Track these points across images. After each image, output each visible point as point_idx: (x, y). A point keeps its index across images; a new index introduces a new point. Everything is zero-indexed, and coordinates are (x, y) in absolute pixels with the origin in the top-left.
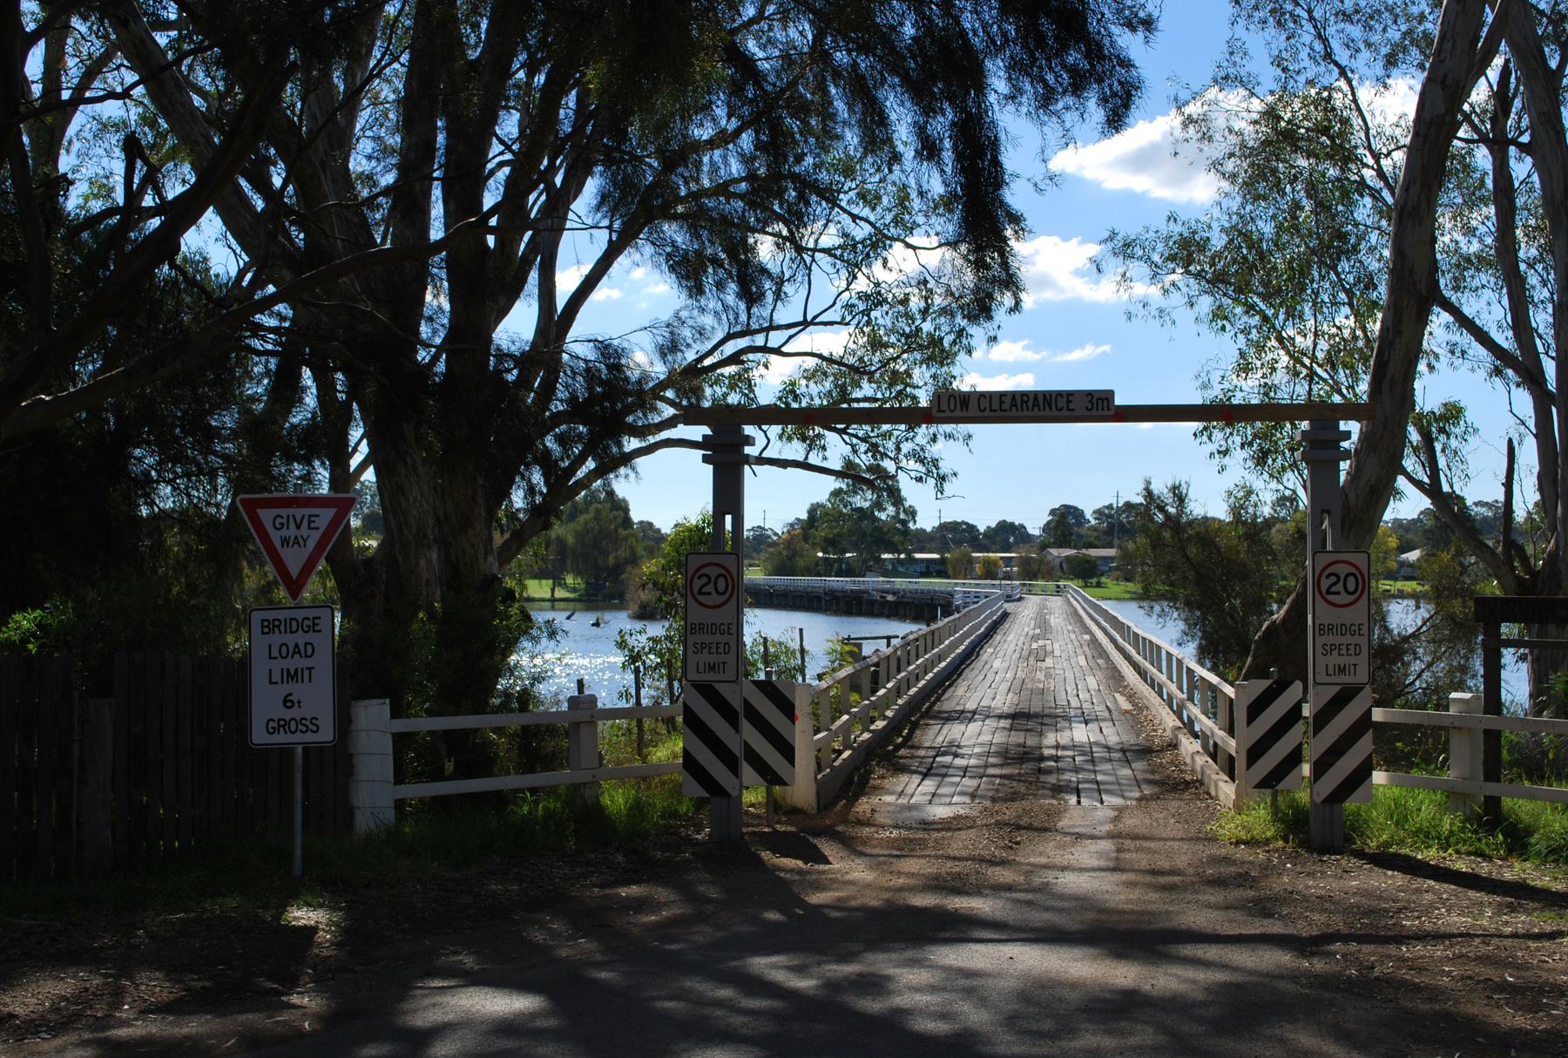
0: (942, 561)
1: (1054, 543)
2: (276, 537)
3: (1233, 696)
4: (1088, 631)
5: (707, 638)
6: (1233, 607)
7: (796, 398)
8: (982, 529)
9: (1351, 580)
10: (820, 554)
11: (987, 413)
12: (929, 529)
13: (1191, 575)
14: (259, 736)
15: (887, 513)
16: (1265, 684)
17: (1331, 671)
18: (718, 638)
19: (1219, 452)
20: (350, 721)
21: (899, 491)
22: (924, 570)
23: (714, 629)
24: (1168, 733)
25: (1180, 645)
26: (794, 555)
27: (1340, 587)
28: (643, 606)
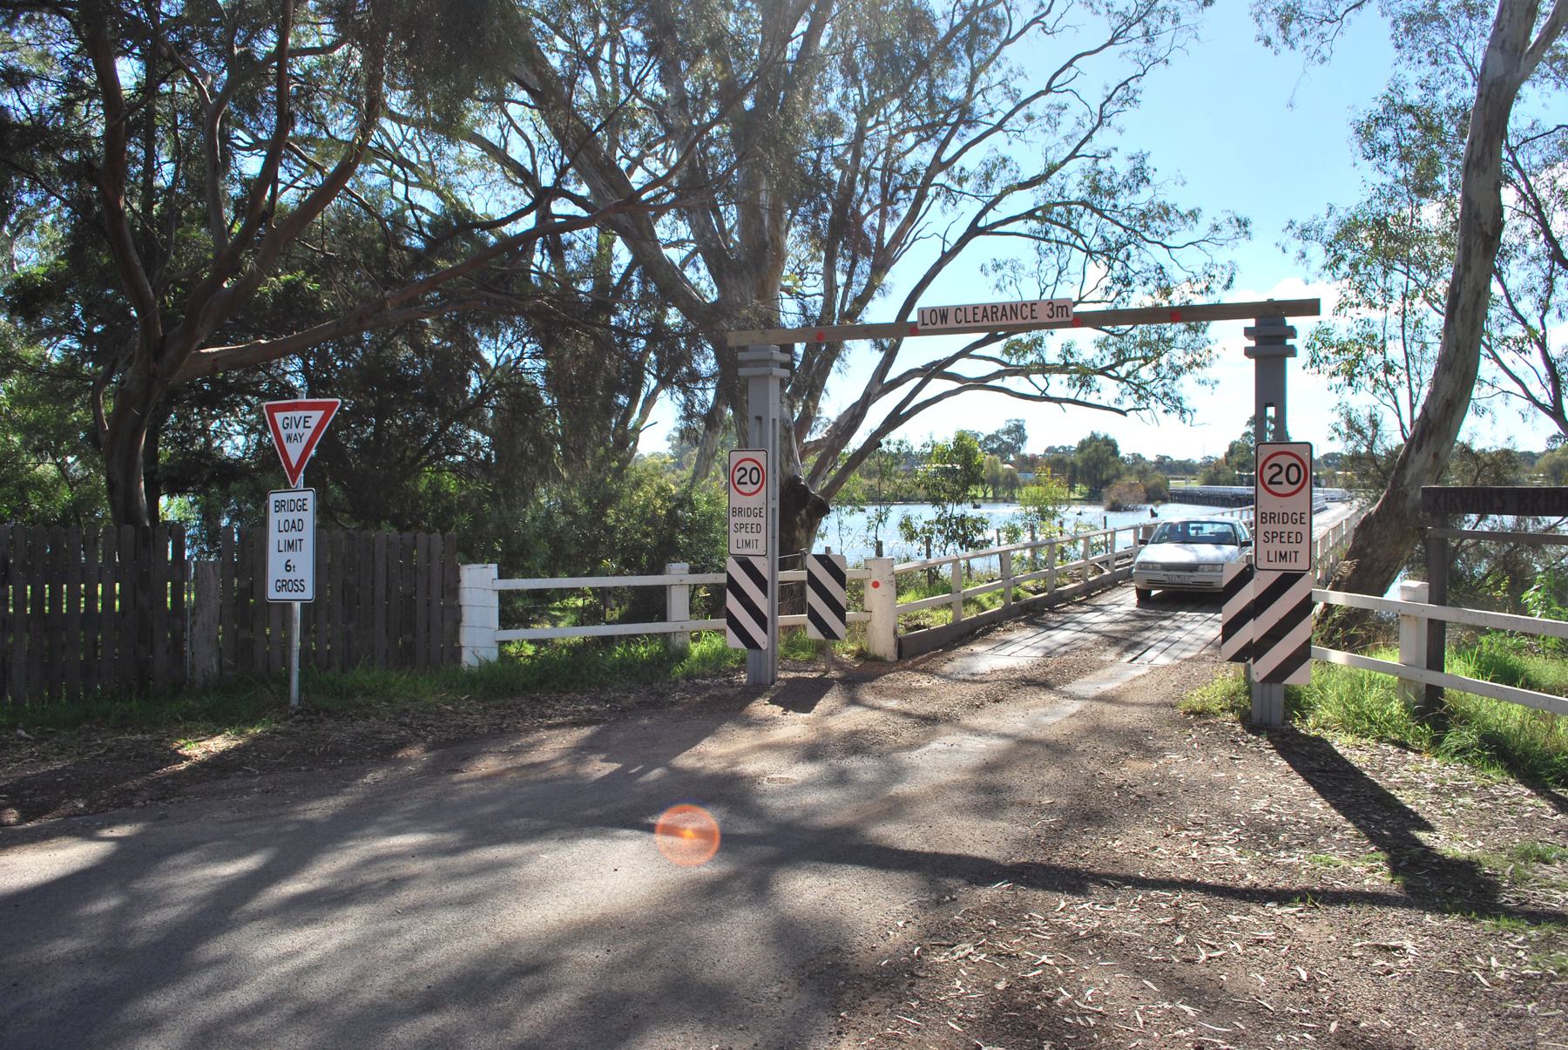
2: (283, 433)
5: (1279, 528)
7: (1071, 355)
9: (1293, 471)
11: (963, 324)
14: (272, 594)
17: (1272, 557)
18: (1289, 527)
20: (459, 581)
23: (1285, 518)
26: (1219, 473)
27: (1281, 478)
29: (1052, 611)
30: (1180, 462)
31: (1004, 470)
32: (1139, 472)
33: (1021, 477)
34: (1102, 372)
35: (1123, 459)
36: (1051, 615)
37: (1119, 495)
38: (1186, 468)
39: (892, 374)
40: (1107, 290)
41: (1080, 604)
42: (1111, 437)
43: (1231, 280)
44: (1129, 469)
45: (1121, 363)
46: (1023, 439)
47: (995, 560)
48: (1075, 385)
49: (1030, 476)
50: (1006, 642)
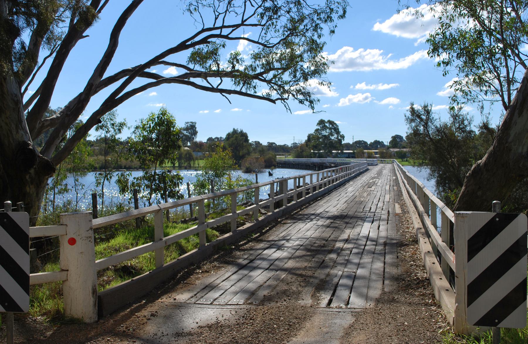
0: (354, 153)
1: (392, 147)
3: (453, 220)
4: (395, 175)
6: (452, 162)
8: (369, 143)
10: (312, 151)
12: (351, 143)
13: (432, 147)
15: (334, 137)
16: (489, 215)
19: (443, 63)
21: (338, 129)
22: (347, 156)
24: (414, 231)
25: (428, 180)
26: (303, 151)
28: (247, 169)
29: (238, 249)
30: (280, 146)
31: (185, 150)
32: (260, 151)
33: (194, 154)
34: (256, 77)
35: (251, 144)
36: (238, 253)
37: (251, 164)
38: (284, 149)
39: (109, 72)
40: (262, 16)
41: (258, 240)
42: (244, 131)
43: (345, 12)
44: (254, 149)
45: (267, 71)
46: (195, 133)
47: (187, 208)
48: (239, 83)
49: (200, 154)
50: (210, 287)
